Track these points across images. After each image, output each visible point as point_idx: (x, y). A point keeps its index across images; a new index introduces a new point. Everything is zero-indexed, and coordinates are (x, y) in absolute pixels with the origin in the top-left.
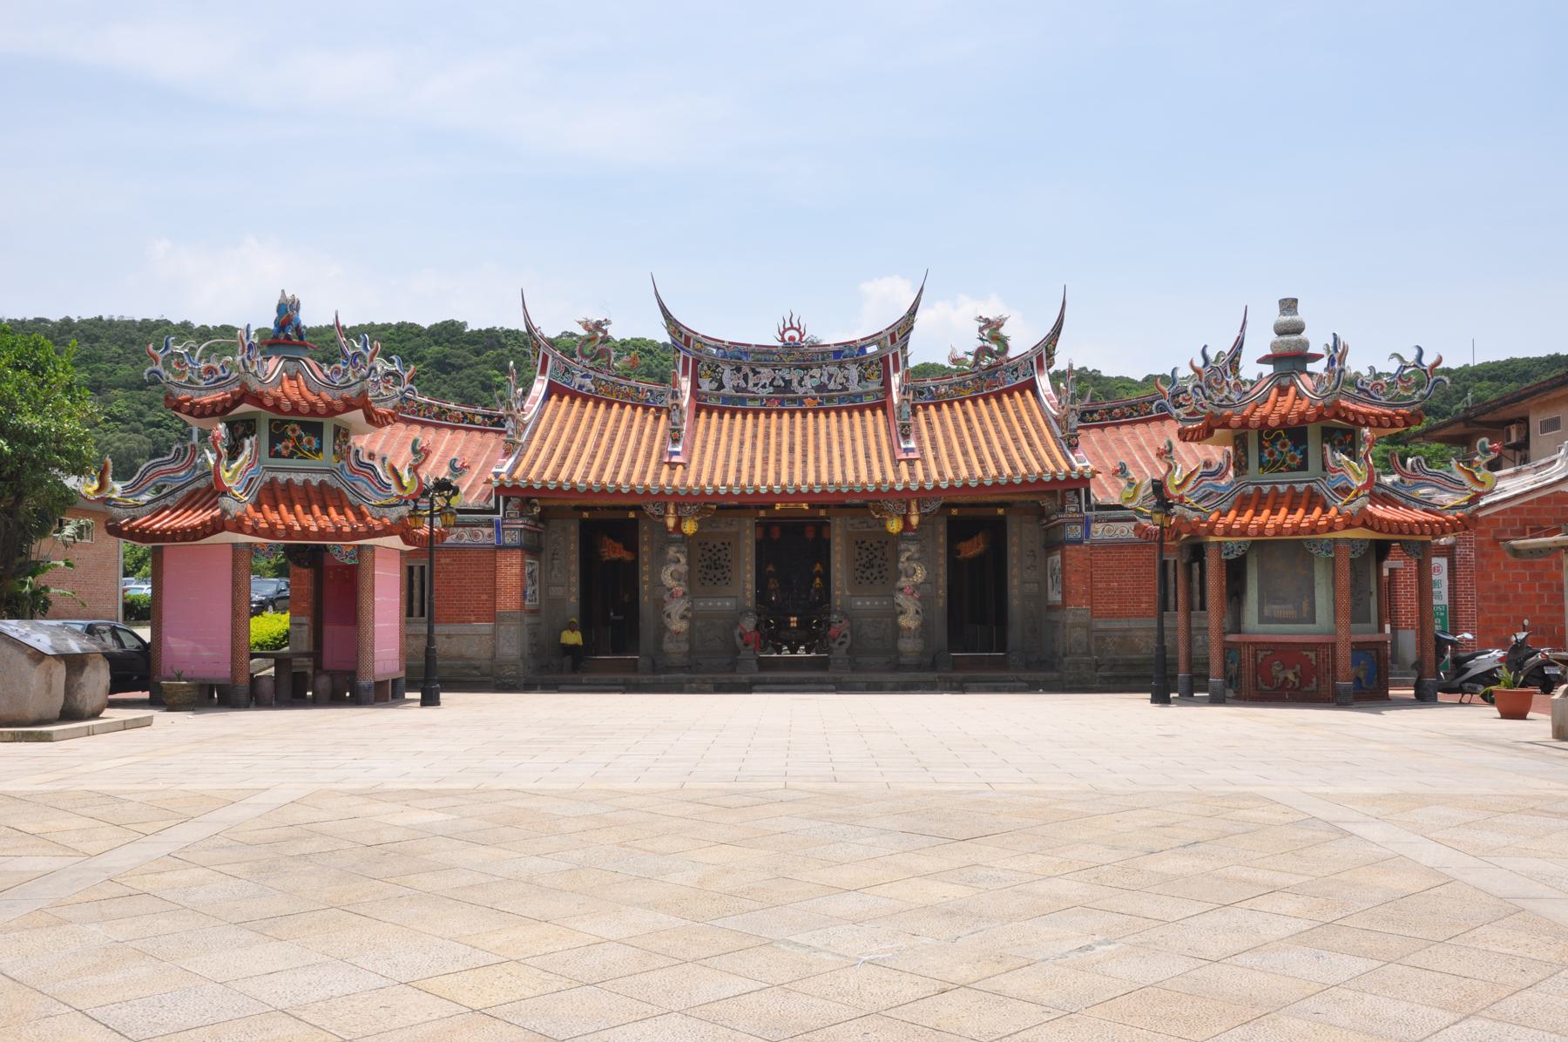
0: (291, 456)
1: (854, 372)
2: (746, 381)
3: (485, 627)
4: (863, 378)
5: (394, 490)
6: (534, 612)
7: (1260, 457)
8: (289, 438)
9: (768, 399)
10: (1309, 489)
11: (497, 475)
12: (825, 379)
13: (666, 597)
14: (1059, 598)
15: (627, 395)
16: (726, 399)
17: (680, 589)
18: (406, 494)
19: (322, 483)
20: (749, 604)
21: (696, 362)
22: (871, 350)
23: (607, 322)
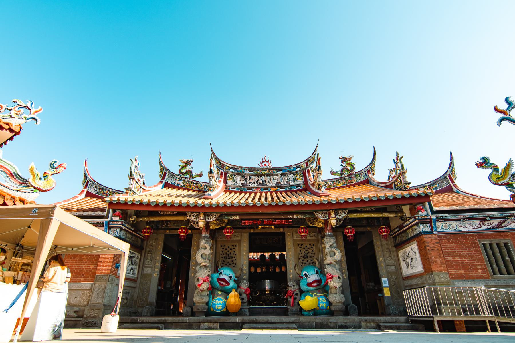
2: (246, 181)
4: (295, 179)
14: (418, 267)
21: (226, 174)
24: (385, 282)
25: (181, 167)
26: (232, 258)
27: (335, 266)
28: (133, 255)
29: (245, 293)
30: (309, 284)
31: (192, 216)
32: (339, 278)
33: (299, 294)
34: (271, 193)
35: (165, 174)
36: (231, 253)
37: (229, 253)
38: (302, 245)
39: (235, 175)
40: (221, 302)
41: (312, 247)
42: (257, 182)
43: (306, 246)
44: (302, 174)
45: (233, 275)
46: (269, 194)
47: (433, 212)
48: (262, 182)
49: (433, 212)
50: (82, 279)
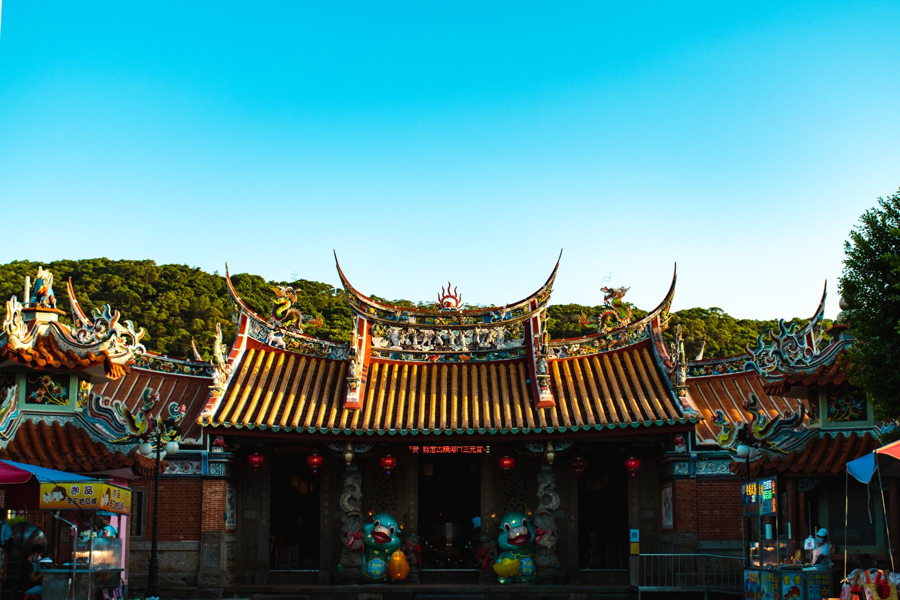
0: (43, 402)
3: (191, 544)
5: (128, 430)
7: (829, 409)
8: (42, 387)
10: (868, 435)
11: (205, 420)
13: (344, 519)
18: (138, 434)
19: (68, 424)
24: (634, 535)
29: (413, 551)
30: (511, 541)
32: (553, 534)
33: (496, 553)
34: (460, 366)
39: (388, 327)
40: (379, 565)
42: (432, 343)
45: (394, 526)
46: (455, 367)
47: (695, 447)
49: (695, 447)
50: (181, 537)
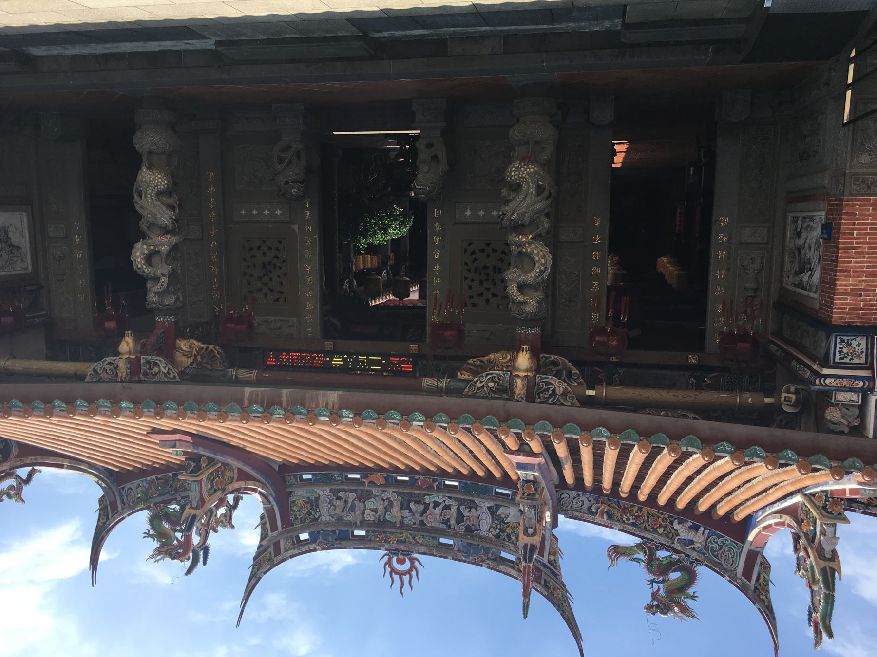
1: (325, 514)
2: (459, 512)
4: (314, 503)
6: (807, 197)
9: (430, 488)
12: (359, 505)
15: (625, 510)
16: (484, 492)
17: (165, 218)
20: (437, 213)
22: (304, 536)
23: (649, 608)
25: (690, 591)
26: (476, 269)
27: (151, 225)
28: (797, 280)
31: (559, 391)
35: (747, 573)
36: (481, 283)
37: (486, 285)
38: (277, 300)
39: (497, 536)
41: (251, 292)
42: (427, 506)
43: (266, 295)
44: (292, 518)
48: (412, 505)
